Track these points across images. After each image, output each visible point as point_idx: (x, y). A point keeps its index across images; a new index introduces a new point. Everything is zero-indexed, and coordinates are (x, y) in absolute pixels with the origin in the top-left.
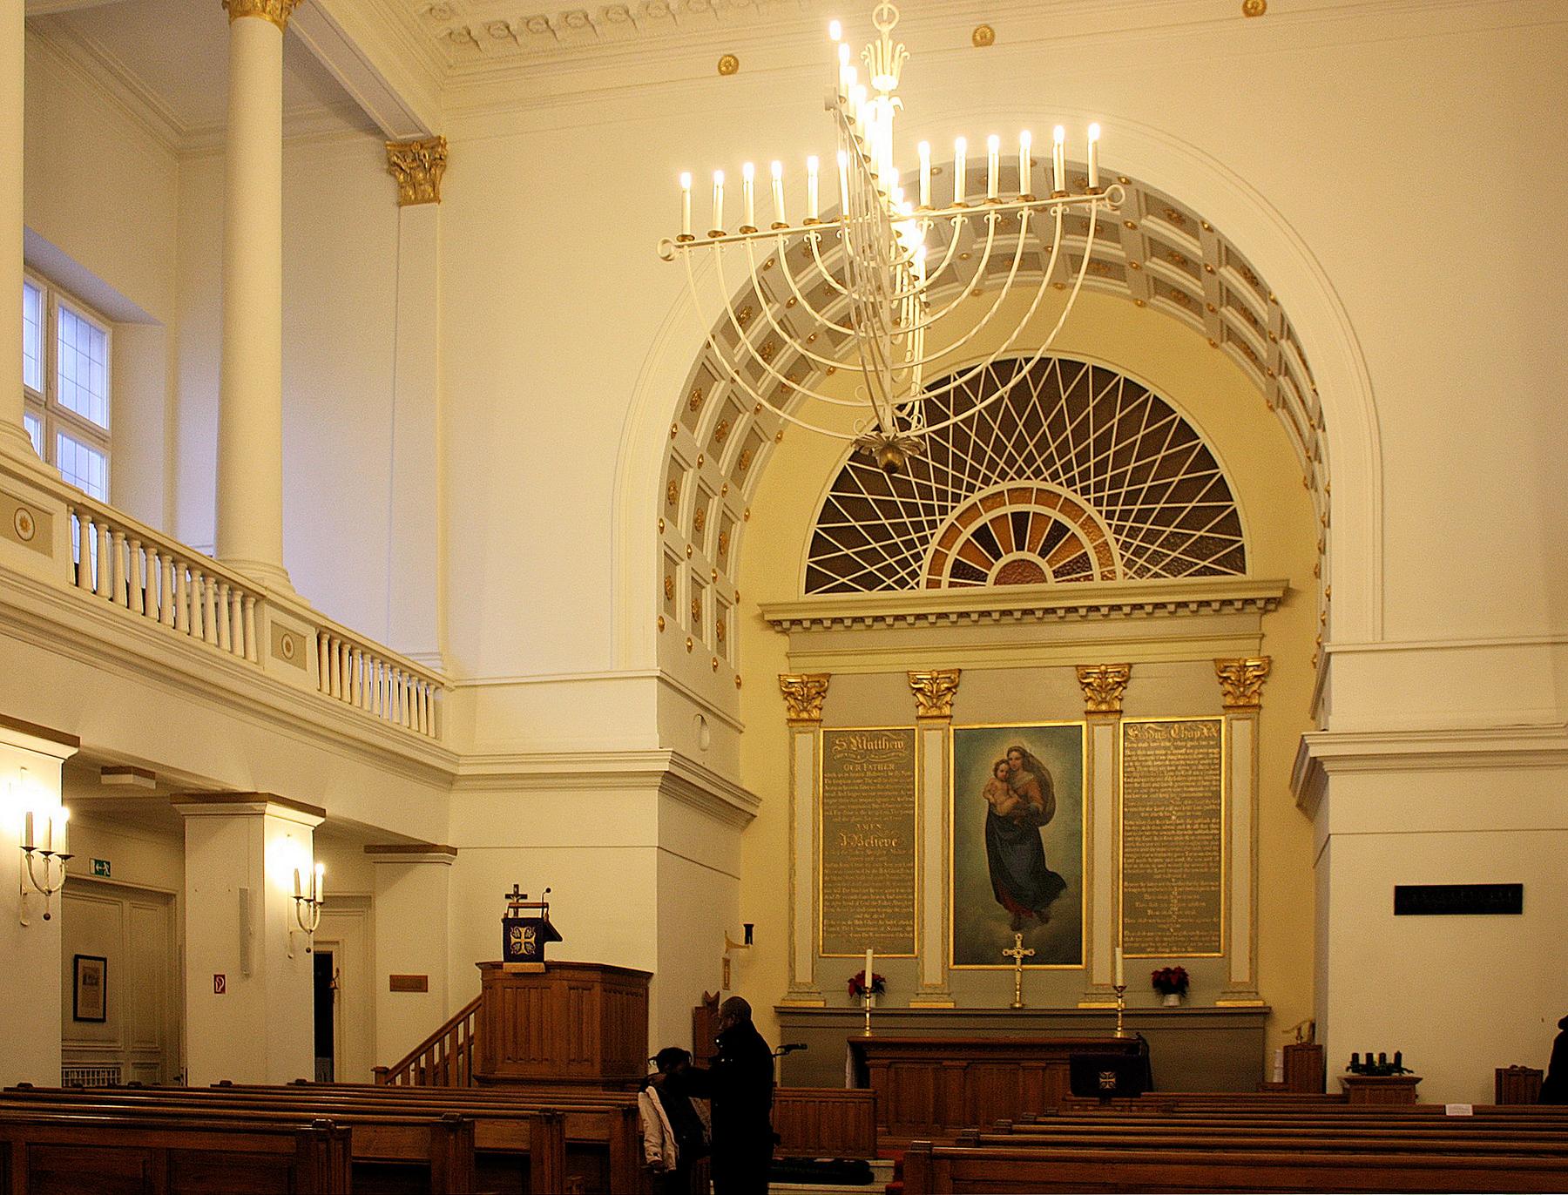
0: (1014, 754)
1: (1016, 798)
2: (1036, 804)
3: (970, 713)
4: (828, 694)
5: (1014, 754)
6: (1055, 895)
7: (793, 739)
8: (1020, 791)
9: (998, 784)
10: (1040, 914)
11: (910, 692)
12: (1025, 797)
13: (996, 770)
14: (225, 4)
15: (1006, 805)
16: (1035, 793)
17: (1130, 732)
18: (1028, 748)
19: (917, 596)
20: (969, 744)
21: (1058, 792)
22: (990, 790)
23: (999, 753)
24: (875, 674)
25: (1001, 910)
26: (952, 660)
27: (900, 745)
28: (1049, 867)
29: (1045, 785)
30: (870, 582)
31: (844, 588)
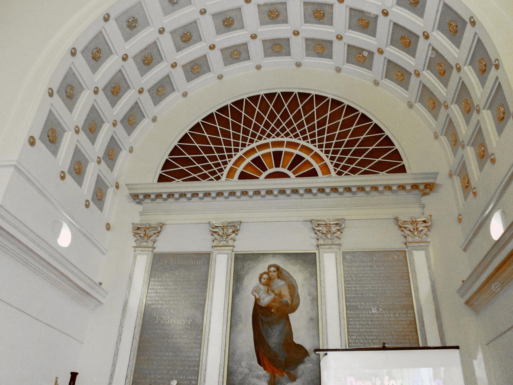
0: (273, 269)
1: (272, 296)
2: (287, 298)
3: (244, 244)
4: (240, 233)
5: (273, 269)
6: (301, 361)
7: (135, 258)
8: (277, 292)
9: (262, 287)
10: (289, 374)
11: (210, 233)
12: (280, 295)
13: (260, 278)
14: (170, 2)
15: (266, 300)
16: (285, 292)
17: (347, 257)
18: (281, 266)
19: (224, 184)
20: (242, 261)
21: (302, 292)
22: (256, 290)
23: (262, 267)
24: (188, 222)
25: (261, 371)
26: (234, 217)
27: (347, 257)
28: (297, 340)
29: (292, 288)
30: (204, 177)
31: (194, 179)
